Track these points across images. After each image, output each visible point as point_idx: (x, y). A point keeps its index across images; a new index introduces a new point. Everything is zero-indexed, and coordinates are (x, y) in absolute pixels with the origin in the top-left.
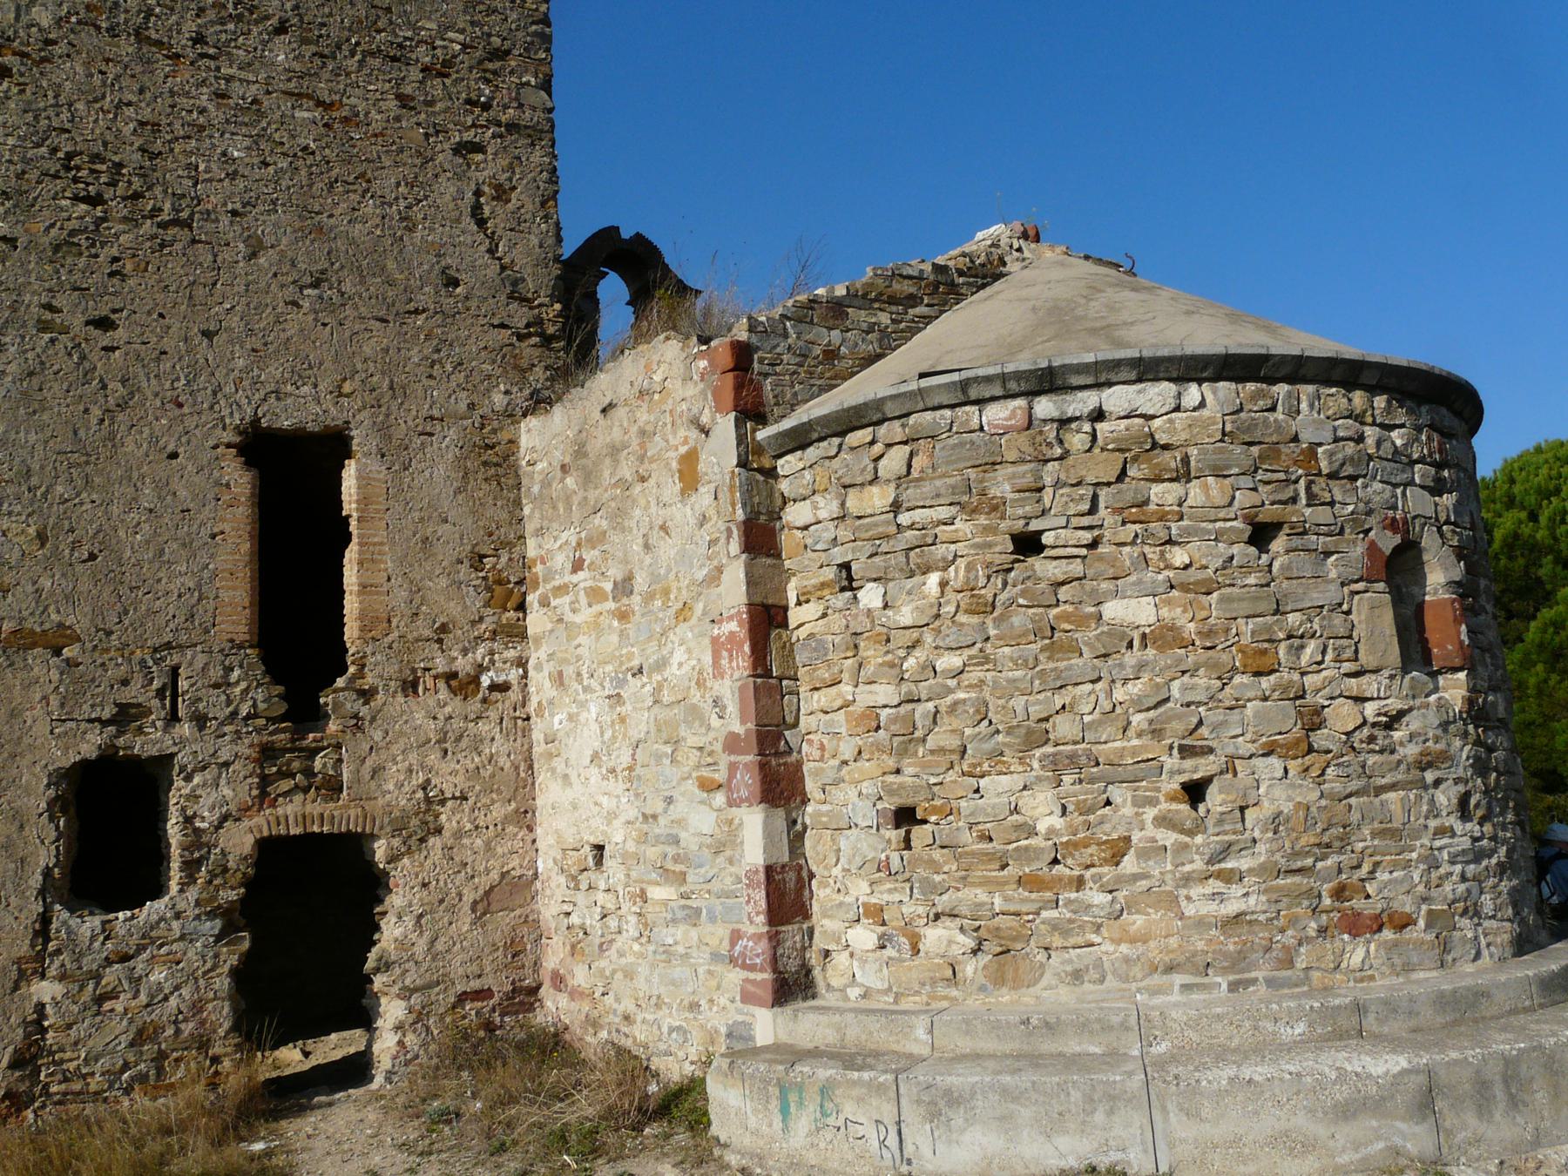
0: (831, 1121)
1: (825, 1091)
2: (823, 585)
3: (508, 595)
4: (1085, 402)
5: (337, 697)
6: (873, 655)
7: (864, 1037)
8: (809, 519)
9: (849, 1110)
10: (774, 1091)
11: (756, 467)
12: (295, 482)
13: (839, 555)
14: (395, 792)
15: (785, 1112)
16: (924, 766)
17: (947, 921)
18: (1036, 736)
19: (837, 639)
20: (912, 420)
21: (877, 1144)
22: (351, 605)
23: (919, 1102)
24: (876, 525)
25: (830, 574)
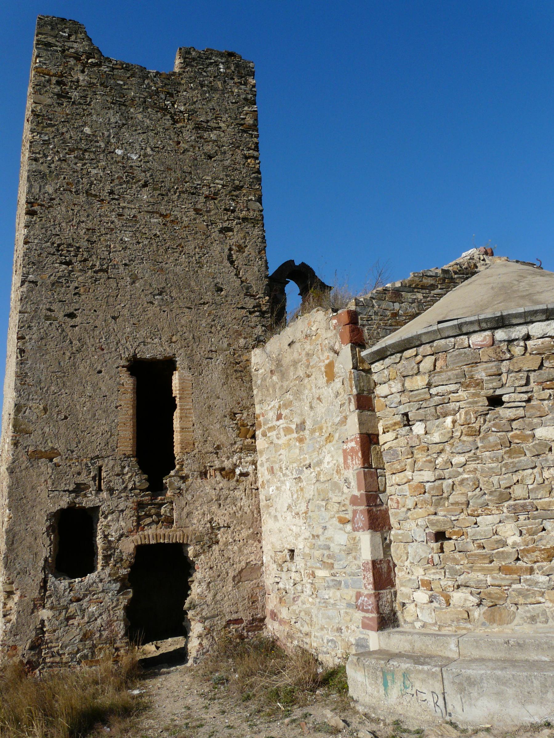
0: (409, 691)
1: (406, 675)
2: (395, 424)
3: (248, 431)
4: (519, 332)
5: (170, 480)
6: (421, 457)
7: (424, 648)
8: (387, 392)
9: (418, 685)
10: (379, 674)
11: (362, 369)
12: (152, 381)
13: (402, 409)
14: (197, 524)
15: (385, 685)
16: (448, 511)
17: (464, 589)
18: (504, 496)
19: (403, 449)
20: (435, 344)
21: (433, 704)
22: (177, 437)
23: (453, 683)
24: (420, 394)
25: (398, 418)
